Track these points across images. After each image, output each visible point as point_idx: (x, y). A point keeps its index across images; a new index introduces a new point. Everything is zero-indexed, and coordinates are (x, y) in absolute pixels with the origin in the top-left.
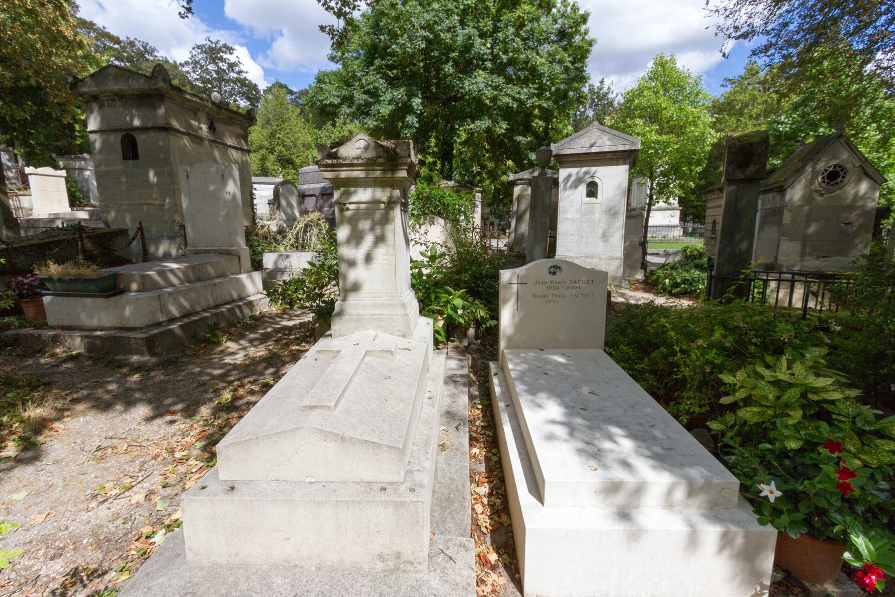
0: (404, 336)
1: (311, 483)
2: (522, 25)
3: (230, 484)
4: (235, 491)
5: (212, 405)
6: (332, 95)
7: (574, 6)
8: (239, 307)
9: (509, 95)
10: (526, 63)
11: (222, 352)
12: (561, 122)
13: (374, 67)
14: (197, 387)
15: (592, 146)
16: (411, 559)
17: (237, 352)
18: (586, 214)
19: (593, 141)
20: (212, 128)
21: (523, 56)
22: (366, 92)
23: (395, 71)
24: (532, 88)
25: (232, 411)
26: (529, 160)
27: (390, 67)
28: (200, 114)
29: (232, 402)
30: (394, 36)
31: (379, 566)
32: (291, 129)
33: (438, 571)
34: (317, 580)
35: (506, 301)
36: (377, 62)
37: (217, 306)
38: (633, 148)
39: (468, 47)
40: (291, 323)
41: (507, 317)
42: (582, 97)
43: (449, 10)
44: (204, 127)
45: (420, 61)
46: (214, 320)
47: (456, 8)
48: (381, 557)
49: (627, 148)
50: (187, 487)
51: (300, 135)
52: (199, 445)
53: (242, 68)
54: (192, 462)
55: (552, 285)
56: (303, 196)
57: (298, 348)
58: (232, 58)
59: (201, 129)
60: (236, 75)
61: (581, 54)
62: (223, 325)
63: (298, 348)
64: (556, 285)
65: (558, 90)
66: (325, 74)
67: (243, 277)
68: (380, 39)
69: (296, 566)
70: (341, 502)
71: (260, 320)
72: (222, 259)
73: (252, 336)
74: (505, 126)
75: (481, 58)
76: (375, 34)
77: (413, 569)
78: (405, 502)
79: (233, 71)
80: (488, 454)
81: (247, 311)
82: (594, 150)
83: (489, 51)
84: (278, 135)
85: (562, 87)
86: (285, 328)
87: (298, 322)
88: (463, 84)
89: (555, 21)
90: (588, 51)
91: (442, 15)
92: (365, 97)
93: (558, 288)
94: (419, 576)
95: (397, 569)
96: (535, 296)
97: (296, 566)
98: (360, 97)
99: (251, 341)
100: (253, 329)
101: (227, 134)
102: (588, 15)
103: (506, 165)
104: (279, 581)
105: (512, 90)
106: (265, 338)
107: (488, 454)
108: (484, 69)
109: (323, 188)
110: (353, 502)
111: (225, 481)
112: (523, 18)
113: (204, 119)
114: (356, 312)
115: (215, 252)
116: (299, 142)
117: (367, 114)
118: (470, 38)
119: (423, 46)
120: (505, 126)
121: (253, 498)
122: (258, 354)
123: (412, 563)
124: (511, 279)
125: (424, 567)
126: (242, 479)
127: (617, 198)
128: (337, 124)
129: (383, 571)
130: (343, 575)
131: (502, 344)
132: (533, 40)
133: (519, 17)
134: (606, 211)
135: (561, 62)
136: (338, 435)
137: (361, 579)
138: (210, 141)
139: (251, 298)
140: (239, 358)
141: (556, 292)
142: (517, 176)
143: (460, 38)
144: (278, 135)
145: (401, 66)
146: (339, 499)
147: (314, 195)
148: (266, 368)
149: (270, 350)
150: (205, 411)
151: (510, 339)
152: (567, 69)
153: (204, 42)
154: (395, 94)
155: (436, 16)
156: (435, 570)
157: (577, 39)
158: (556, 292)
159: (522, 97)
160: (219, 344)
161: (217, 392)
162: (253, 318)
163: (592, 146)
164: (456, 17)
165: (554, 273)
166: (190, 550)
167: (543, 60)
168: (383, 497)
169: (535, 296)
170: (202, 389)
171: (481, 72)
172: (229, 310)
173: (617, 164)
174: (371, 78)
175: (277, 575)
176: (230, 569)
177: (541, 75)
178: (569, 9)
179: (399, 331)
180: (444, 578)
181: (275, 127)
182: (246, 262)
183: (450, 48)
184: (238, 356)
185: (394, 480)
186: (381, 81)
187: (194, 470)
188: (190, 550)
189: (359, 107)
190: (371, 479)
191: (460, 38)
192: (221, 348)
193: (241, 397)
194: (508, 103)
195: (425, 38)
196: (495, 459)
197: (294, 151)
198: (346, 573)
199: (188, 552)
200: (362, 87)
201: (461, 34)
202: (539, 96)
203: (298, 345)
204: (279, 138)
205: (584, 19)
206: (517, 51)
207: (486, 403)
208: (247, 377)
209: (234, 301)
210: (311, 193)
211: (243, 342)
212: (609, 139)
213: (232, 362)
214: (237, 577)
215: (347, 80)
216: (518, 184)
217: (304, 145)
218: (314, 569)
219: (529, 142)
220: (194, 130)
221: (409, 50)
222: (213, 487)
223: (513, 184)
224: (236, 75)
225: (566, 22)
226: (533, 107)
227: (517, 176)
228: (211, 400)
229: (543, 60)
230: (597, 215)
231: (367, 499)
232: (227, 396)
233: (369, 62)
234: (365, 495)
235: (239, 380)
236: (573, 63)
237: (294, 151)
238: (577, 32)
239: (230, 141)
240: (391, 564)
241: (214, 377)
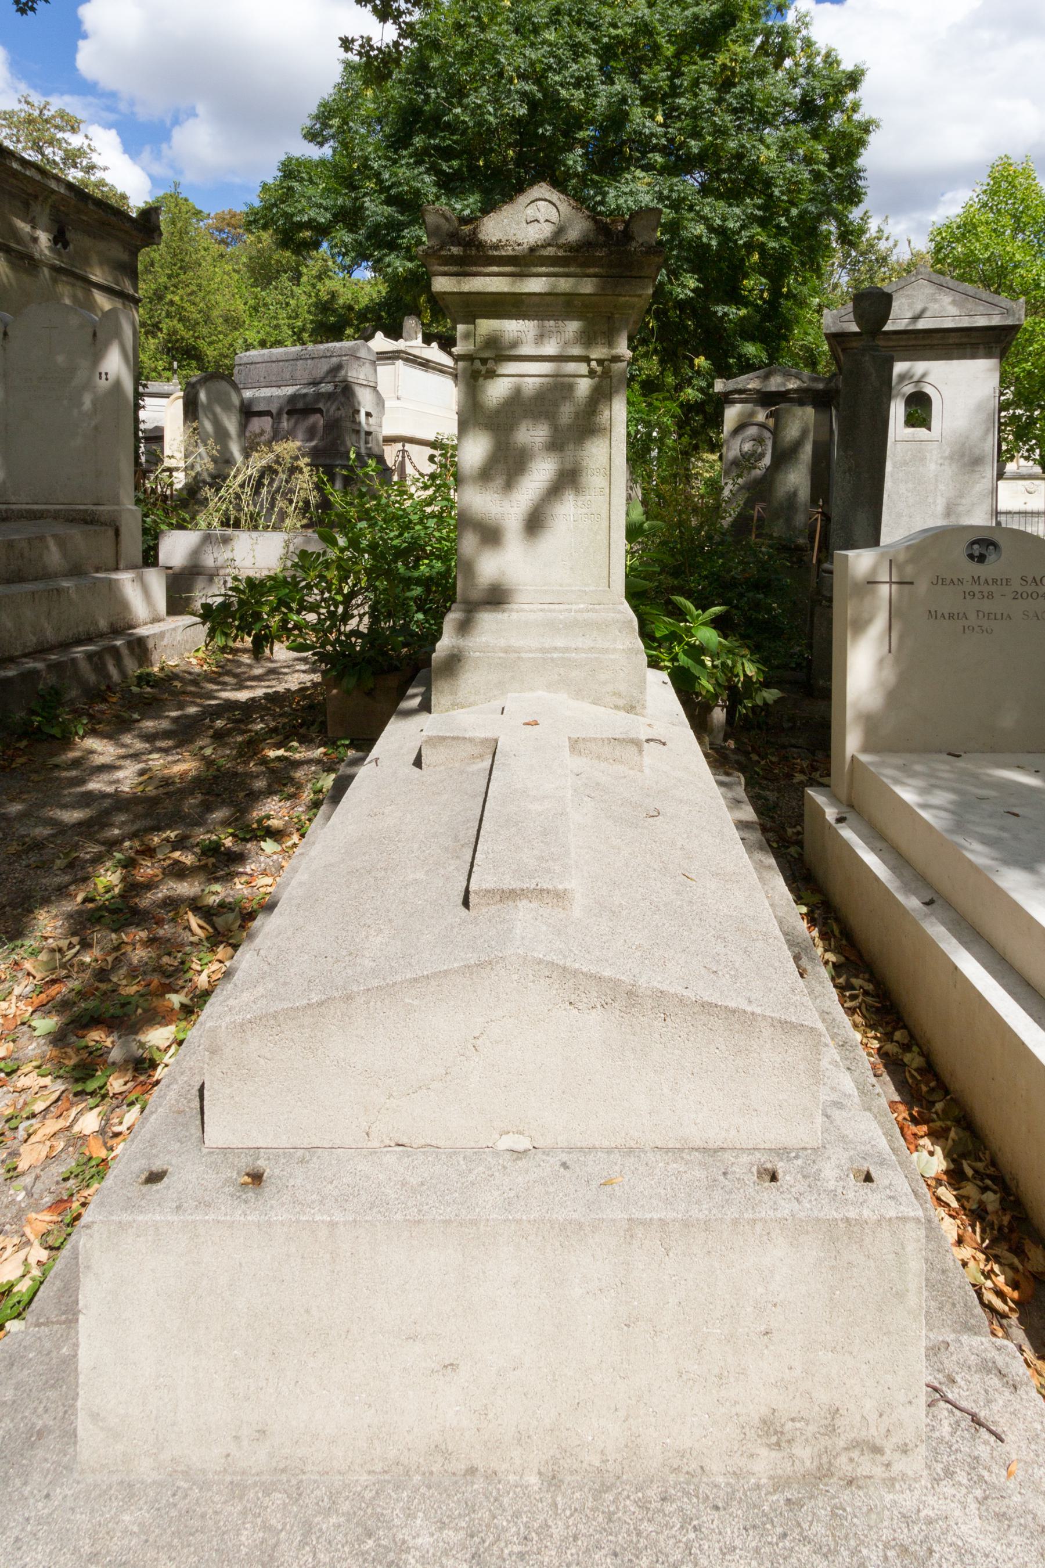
0: (631, 709)
1: (518, 1154)
2: (727, 85)
3: (244, 1163)
4: (268, 1188)
5: (69, 907)
6: (313, 204)
7: (828, 55)
8: (115, 652)
9: (705, 219)
10: (740, 156)
11: (76, 763)
12: (804, 283)
13: (411, 149)
14: (18, 855)
15: (916, 318)
16: (874, 1433)
17: (116, 764)
18: (906, 463)
19: (919, 307)
20: (59, 239)
21: (732, 145)
22: (388, 202)
23: (455, 163)
24: (752, 204)
25: (127, 924)
26: (740, 356)
27: (447, 154)
28: (36, 208)
29: (122, 896)
30: (458, 92)
31: (764, 1463)
32: (199, 286)
33: (962, 1477)
34: (558, 1530)
35: (860, 626)
36: (418, 141)
37: (65, 646)
38: (1009, 322)
39: (617, 118)
40: (243, 696)
41: (864, 670)
42: (852, 233)
43: (580, 44)
44: (44, 238)
45: (509, 146)
46: (52, 680)
47: (594, 40)
48: (773, 1431)
49: (996, 321)
50: (23, 1166)
51: (219, 298)
52: (46, 1024)
53: (96, 159)
54: (29, 1080)
55: (976, 588)
56: (247, 412)
57: (281, 752)
58: (76, 141)
59: (35, 240)
60: (80, 175)
61: (848, 146)
62: (74, 693)
63: (281, 752)
64: (986, 589)
65: (802, 216)
66: (299, 163)
67: (126, 579)
68: (428, 95)
69: (472, 1471)
70: (643, 1223)
71: (168, 687)
72: (76, 535)
73: (149, 725)
74: (692, 283)
75: (644, 144)
76: (418, 85)
77: (878, 1471)
78: (862, 1223)
79: (75, 166)
80: (890, 1047)
81: (131, 666)
82: (922, 325)
83: (660, 130)
84: (169, 297)
85: (812, 208)
86: (231, 705)
87: (259, 692)
88: (605, 194)
89: (793, 81)
90: (862, 143)
91: (564, 53)
92: (388, 210)
93: (990, 596)
94: (907, 1501)
95: (823, 1473)
96: (933, 615)
97: (472, 1471)
98: (376, 209)
99: (150, 738)
100: (151, 706)
101: (94, 259)
102: (863, 73)
103: (692, 365)
104: (425, 1540)
105: (715, 209)
106: (183, 734)
107: (890, 1047)
108: (648, 168)
109: (293, 399)
110: (686, 1224)
111: (225, 1150)
112: (732, 70)
113: (44, 219)
114: (502, 643)
115: (56, 516)
116: (215, 313)
117: (392, 246)
118: (624, 100)
119: (523, 111)
120: (692, 283)
121: (338, 1217)
122: (177, 769)
123: (877, 1450)
124: (874, 570)
125: (914, 1464)
126: (284, 1142)
127: (978, 433)
128: (304, 279)
129: (779, 1484)
130: (643, 1505)
131: (852, 742)
132: (755, 114)
133: (724, 67)
134: (951, 458)
135: (808, 160)
136: (617, 983)
137: (709, 1519)
138: (54, 269)
139: (142, 631)
140: (127, 778)
141: (986, 606)
142: (732, 384)
143: (601, 102)
144: (169, 297)
145: (468, 153)
146: (637, 1214)
147: (268, 413)
148: (208, 807)
149: (204, 758)
150: (49, 924)
151: (871, 723)
152: (817, 177)
153: (17, 107)
154: (458, 206)
155: (552, 54)
156: (949, 1473)
157: (837, 119)
158: (986, 606)
159: (731, 224)
160: (66, 741)
161: (80, 872)
162: (145, 679)
163: (916, 318)
164: (594, 60)
165: (981, 559)
166: (95, 1417)
167: (773, 154)
168: (773, 1203)
169: (933, 615)
170: (33, 858)
171: (639, 173)
172: (90, 656)
173: (973, 357)
174: (403, 172)
175: (411, 1516)
176: (237, 1490)
177: (768, 183)
178: (818, 60)
179: (619, 695)
180: (994, 1506)
181: (163, 279)
182: (133, 544)
183: (575, 121)
184: (120, 774)
185: (791, 1142)
186: (427, 179)
187: (39, 1107)
188: (95, 1417)
189: (374, 233)
190: (715, 1137)
191: (601, 102)
192: (72, 755)
193: (150, 885)
194: (700, 237)
195: (524, 95)
196: (913, 1060)
197: (205, 331)
198: (653, 1493)
199: (83, 1425)
200: (383, 189)
201: (604, 95)
202: (763, 222)
203: (278, 746)
204: (172, 303)
205: (854, 80)
206: (720, 131)
207: (816, 899)
208: (158, 828)
209: (102, 635)
210: (262, 407)
211: (127, 739)
212: (954, 303)
213: (110, 789)
214: (266, 1527)
215: (346, 176)
216: (733, 402)
217: (226, 321)
218: (533, 1480)
219: (742, 319)
220: (19, 240)
221: (491, 119)
222: (188, 1173)
223: (726, 399)
224: (80, 175)
225: (816, 84)
226: (750, 246)
227: (732, 384)
228: (62, 892)
229: (773, 154)
230: (933, 467)
231: (732, 1212)
232: (108, 879)
233: (398, 141)
234: (718, 1195)
235: (133, 836)
236: (831, 166)
237: (205, 331)
238: (838, 106)
239: (97, 276)
240: (805, 1454)
241: (62, 829)
